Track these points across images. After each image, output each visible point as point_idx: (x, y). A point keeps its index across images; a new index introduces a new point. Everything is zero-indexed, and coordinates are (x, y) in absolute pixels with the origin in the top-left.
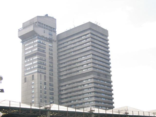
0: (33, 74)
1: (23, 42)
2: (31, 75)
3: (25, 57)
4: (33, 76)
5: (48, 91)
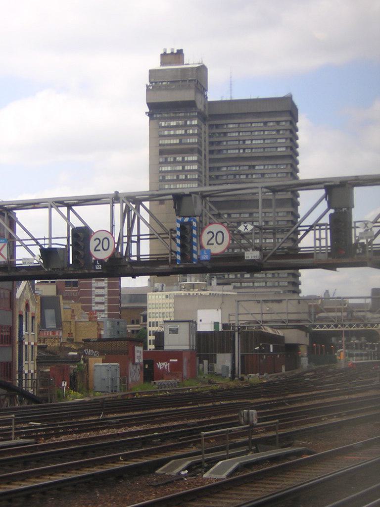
1: (150, 114)
3: (160, 150)
5: (154, 306)
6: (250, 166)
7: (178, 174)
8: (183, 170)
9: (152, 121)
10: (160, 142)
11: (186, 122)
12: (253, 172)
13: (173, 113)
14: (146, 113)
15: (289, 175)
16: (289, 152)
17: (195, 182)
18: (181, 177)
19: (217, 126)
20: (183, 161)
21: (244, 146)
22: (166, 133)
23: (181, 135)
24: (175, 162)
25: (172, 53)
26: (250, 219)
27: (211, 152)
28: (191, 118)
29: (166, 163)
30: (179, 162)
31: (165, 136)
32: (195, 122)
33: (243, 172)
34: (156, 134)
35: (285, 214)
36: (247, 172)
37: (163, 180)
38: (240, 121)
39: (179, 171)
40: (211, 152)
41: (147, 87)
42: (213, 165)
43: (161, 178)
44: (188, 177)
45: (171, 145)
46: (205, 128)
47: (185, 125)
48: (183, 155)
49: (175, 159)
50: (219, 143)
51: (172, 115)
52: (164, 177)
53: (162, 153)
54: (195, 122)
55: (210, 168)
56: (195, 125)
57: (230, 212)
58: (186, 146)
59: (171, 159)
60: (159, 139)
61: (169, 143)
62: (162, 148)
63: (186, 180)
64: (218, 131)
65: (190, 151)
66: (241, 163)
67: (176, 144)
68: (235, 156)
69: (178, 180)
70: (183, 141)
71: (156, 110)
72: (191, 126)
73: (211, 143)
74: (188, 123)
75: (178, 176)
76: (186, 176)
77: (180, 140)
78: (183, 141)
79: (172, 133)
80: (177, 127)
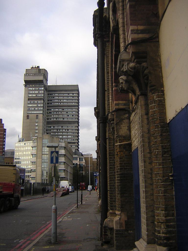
0: (37, 114)
1: (25, 86)
2: (36, 115)
3: (28, 98)
4: (37, 116)
6: (62, 126)
7: (35, 108)
8: (37, 106)
9: (26, 88)
10: (29, 89)
11: (39, 88)
12: (64, 111)
13: (34, 85)
14: (24, 85)
15: (77, 140)
16: (77, 104)
17: (42, 111)
18: (35, 102)
19: (51, 94)
20: (37, 103)
21: (60, 102)
22: (31, 92)
23: (37, 93)
24: (34, 103)
25: (35, 67)
26: (62, 128)
27: (48, 103)
28: (41, 87)
29: (30, 103)
30: (36, 103)
31: (31, 93)
32: (43, 89)
33: (59, 111)
34: (27, 93)
35: (75, 146)
36: (61, 111)
37: (29, 110)
38: (59, 93)
39: (36, 107)
40: (48, 103)
41: (25, 74)
42: (48, 108)
43: (28, 109)
44: (39, 109)
45: (33, 97)
46: (46, 93)
47: (39, 89)
48: (38, 101)
49: (34, 102)
50: (51, 100)
51: (34, 86)
52: (29, 109)
53: (29, 99)
54: (43, 89)
55: (47, 109)
56: (42, 90)
57: (54, 125)
58: (39, 97)
59: (32, 102)
60: (27, 111)
61: (33, 113)
62: (29, 98)
63: (38, 110)
64: (51, 96)
65: (41, 99)
66: (59, 108)
67: (35, 97)
68: (57, 105)
69: (35, 110)
70: (38, 96)
71: (28, 83)
72: (41, 90)
73: (48, 100)
74: (40, 89)
75: (35, 109)
76: (38, 108)
77: (37, 95)
78: (38, 96)
79: (33, 92)
80: (35, 90)
